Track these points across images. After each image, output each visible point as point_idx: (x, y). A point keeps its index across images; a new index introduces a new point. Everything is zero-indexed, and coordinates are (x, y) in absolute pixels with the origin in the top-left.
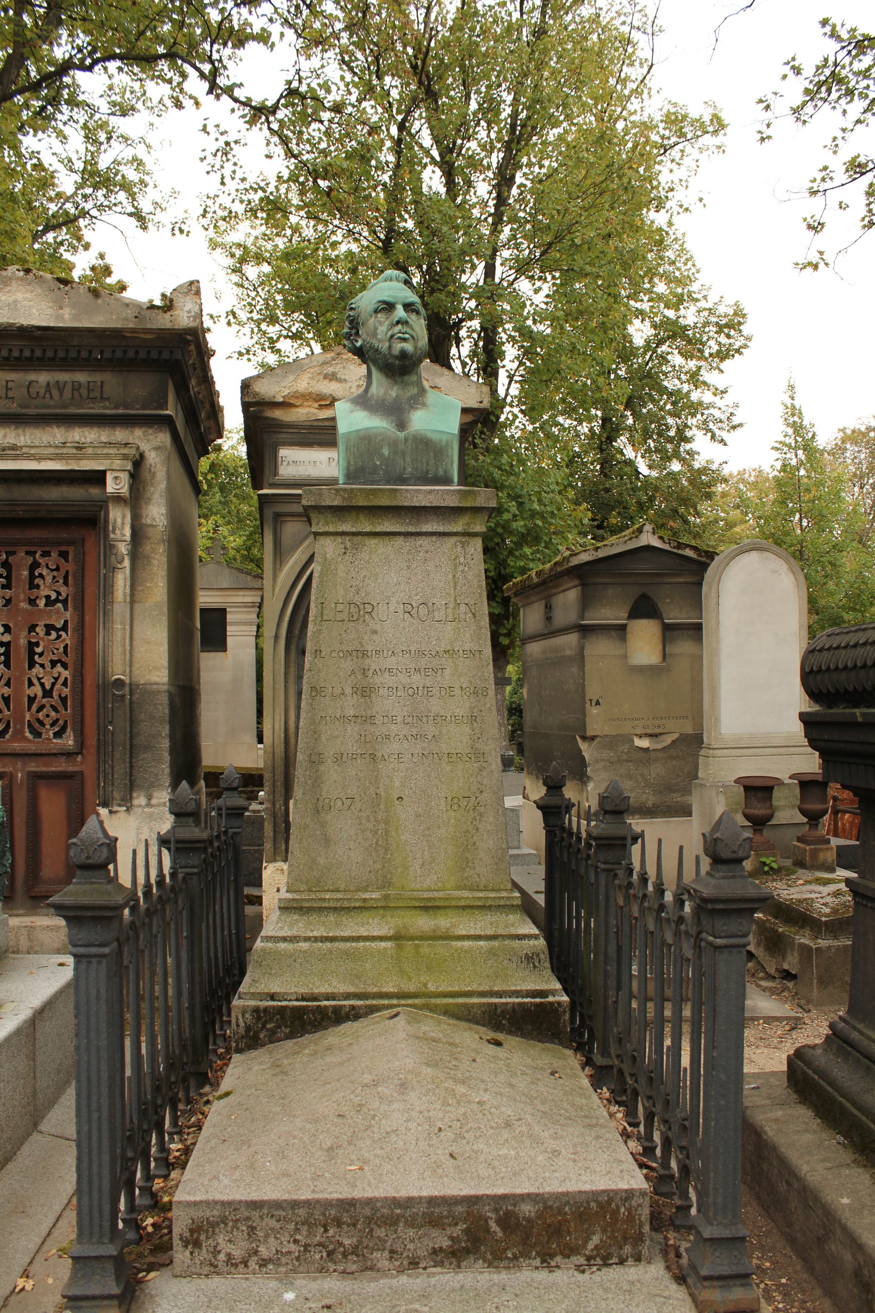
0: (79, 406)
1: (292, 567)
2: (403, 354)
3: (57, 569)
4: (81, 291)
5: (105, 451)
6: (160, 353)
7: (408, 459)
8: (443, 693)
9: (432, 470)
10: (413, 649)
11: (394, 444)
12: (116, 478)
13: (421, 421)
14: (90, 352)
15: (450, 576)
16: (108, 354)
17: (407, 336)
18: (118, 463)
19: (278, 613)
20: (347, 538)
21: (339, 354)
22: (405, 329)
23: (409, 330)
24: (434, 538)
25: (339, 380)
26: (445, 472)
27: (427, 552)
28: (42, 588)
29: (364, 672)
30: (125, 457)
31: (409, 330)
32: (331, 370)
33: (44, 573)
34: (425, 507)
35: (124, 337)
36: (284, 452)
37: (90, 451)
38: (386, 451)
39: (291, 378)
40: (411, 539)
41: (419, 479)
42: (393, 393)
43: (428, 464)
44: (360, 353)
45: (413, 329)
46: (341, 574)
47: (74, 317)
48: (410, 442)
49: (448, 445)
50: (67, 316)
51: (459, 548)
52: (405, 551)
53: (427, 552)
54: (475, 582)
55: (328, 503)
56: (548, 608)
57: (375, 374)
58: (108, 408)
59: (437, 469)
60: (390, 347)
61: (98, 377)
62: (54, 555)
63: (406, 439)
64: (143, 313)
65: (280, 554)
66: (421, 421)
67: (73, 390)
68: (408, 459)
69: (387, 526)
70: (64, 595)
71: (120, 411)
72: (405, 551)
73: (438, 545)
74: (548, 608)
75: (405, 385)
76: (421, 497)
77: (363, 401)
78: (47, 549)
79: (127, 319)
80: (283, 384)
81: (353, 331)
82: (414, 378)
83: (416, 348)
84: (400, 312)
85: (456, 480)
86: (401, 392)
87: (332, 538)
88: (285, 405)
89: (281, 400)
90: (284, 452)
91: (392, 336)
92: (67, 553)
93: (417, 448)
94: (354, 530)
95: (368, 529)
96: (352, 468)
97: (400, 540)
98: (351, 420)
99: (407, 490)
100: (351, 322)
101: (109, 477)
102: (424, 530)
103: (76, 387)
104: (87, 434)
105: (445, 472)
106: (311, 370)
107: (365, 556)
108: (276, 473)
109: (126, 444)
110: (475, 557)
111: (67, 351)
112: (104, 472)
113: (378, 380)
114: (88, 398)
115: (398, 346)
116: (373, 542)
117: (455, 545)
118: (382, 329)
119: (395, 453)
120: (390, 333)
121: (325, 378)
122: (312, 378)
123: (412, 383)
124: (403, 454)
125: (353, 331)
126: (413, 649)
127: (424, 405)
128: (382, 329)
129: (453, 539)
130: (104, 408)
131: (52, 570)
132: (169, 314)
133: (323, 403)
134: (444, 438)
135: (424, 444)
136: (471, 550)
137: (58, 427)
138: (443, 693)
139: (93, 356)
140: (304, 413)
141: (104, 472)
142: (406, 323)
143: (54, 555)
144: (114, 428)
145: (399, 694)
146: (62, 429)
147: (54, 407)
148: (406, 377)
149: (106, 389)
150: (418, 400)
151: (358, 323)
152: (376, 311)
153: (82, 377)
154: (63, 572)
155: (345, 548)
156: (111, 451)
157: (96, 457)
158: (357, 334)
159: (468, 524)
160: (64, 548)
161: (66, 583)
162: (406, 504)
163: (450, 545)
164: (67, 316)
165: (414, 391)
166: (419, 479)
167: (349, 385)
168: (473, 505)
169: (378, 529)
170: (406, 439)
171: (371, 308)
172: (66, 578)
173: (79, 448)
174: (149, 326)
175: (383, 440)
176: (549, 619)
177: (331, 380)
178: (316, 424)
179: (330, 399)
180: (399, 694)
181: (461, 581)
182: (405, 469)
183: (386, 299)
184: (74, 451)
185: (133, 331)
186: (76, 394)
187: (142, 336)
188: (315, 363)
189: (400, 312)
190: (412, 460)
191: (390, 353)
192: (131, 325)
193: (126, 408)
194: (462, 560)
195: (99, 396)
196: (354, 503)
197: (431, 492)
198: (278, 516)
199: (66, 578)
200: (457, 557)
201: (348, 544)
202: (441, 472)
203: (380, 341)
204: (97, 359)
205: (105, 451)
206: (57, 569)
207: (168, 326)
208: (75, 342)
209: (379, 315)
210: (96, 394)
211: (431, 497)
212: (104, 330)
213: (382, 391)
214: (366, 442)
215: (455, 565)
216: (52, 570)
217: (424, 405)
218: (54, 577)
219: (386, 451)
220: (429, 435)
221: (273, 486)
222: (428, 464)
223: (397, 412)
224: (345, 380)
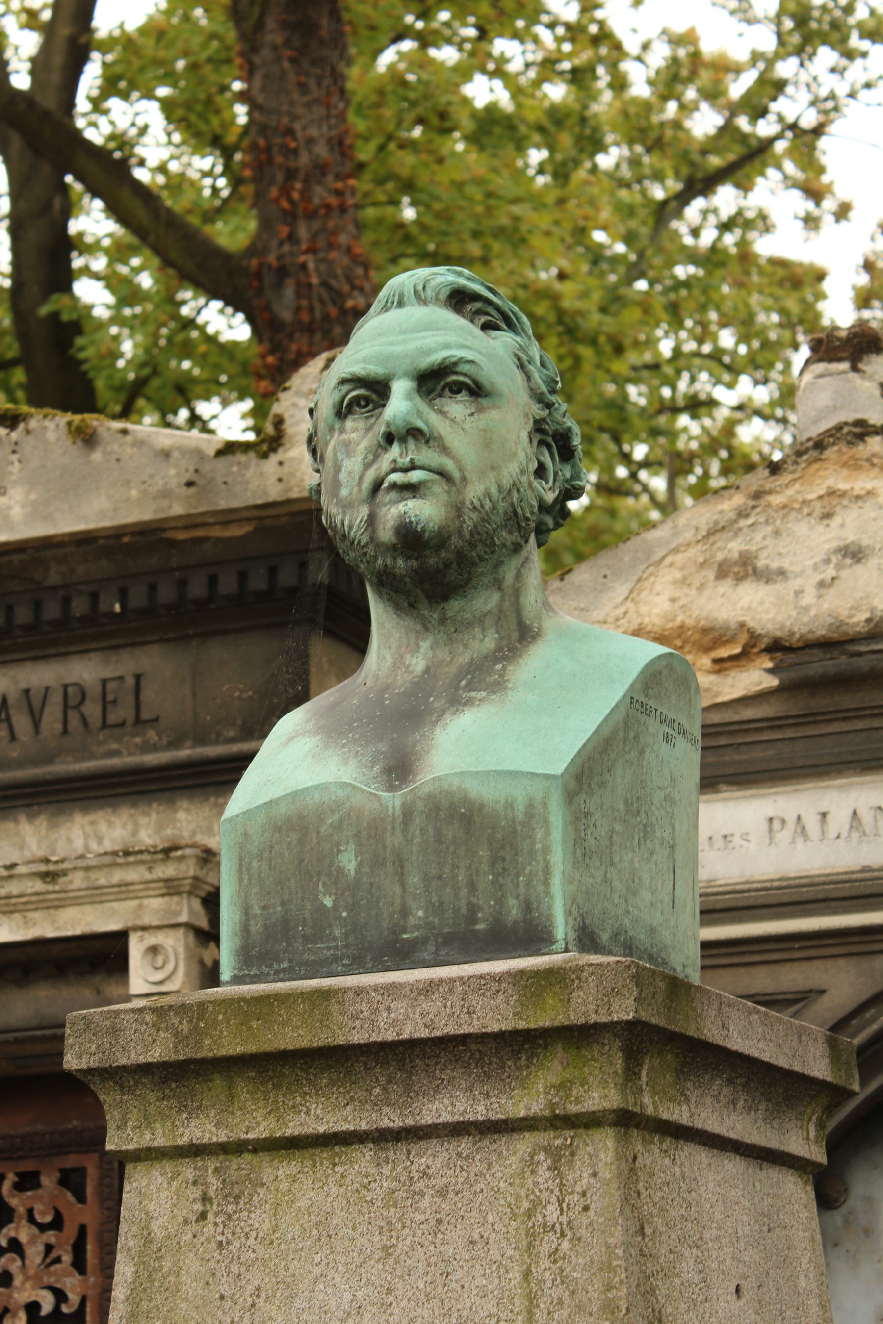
0: (85, 753)
3: (57, 1224)
4: (51, 436)
5: (118, 876)
6: (273, 571)
7: (414, 879)
9: (486, 904)
11: (371, 833)
12: (154, 950)
14: (94, 597)
15: (515, 1275)
16: (138, 598)
17: (415, 476)
18: (154, 907)
20: (211, 1164)
21: (758, 495)
24: (465, 1145)
25: (767, 576)
26: (527, 907)
27: (442, 1193)
28: (17, 1281)
30: (171, 888)
32: (734, 547)
33: (23, 1238)
34: (413, 1044)
35: (172, 543)
37: (77, 880)
38: (349, 861)
39: (621, 590)
40: (397, 1152)
41: (448, 940)
43: (472, 887)
45: (445, 449)
46: (190, 1286)
47: (36, 512)
48: (418, 821)
49: (534, 814)
50: (17, 512)
51: (543, 1174)
52: (377, 1193)
53: (442, 1193)
54: (595, 1294)
55: (136, 1056)
58: (155, 748)
59: (500, 901)
60: (372, 521)
61: (124, 665)
62: (48, 1181)
64: (206, 468)
67: (66, 707)
68: (414, 879)
69: (320, 1115)
70: (74, 1299)
71: (185, 753)
72: (377, 1193)
73: (477, 1166)
75: (453, 629)
76: (400, 1008)
78: (29, 1166)
79: (165, 494)
80: (598, 615)
82: (486, 601)
85: (561, 929)
86: (443, 654)
87: (169, 1166)
91: (377, 486)
92: (81, 1171)
93: (439, 838)
94: (222, 1136)
95: (261, 1132)
96: (256, 927)
97: (363, 1159)
99: (359, 991)
101: (136, 948)
102: (427, 1119)
103: (73, 698)
104: (103, 827)
105: (527, 907)
106: (679, 558)
107: (259, 1220)
109: (167, 851)
110: (597, 1202)
111: (38, 606)
112: (121, 937)
113: (382, 625)
114: (104, 725)
115: (396, 511)
116: (281, 1171)
117: (531, 1163)
119: (377, 863)
120: (371, 475)
121: (723, 571)
122: (684, 582)
123: (480, 621)
124: (400, 862)
129: (523, 1145)
130: (146, 748)
131: (43, 1228)
132: (274, 458)
133: (724, 652)
134: (520, 794)
136: (580, 1176)
137: (31, 817)
139: (103, 607)
141: (121, 937)
143: (48, 1181)
144: (171, 802)
146: (42, 822)
147: (20, 764)
148: (454, 605)
149: (147, 694)
153: (85, 670)
154: (70, 1231)
155: (205, 1199)
156: (133, 875)
157: (95, 895)
159: (563, 1086)
160: (72, 1161)
161: (79, 1265)
162: (357, 1038)
163: (514, 1162)
164: (17, 512)
166: (448, 940)
167: (794, 584)
168: (560, 1020)
169: (293, 1128)
170: (407, 813)
172: (79, 1249)
173: (49, 877)
174: (223, 504)
175: (338, 826)
177: (739, 579)
179: (743, 638)
181: (551, 1292)
182: (405, 912)
184: (39, 886)
185: (190, 522)
186: (73, 716)
187: (217, 532)
188: (688, 535)
189: (401, 403)
190: (426, 879)
192: (178, 510)
193: (201, 741)
194: (552, 1213)
195: (131, 719)
196: (208, 1049)
197: (429, 988)
199: (79, 1249)
200: (537, 1204)
201: (214, 1183)
202: (514, 911)
203: (347, 506)
204: (111, 614)
205: (118, 876)
206: (57, 1224)
207: (274, 493)
208: (54, 577)
209: (349, 424)
210: (123, 712)
211: (431, 1005)
212: (117, 534)
215: (531, 1235)
216: (43, 1228)
218: (49, 1248)
219: (349, 861)
220: (477, 790)
222: (472, 887)
224: (782, 573)
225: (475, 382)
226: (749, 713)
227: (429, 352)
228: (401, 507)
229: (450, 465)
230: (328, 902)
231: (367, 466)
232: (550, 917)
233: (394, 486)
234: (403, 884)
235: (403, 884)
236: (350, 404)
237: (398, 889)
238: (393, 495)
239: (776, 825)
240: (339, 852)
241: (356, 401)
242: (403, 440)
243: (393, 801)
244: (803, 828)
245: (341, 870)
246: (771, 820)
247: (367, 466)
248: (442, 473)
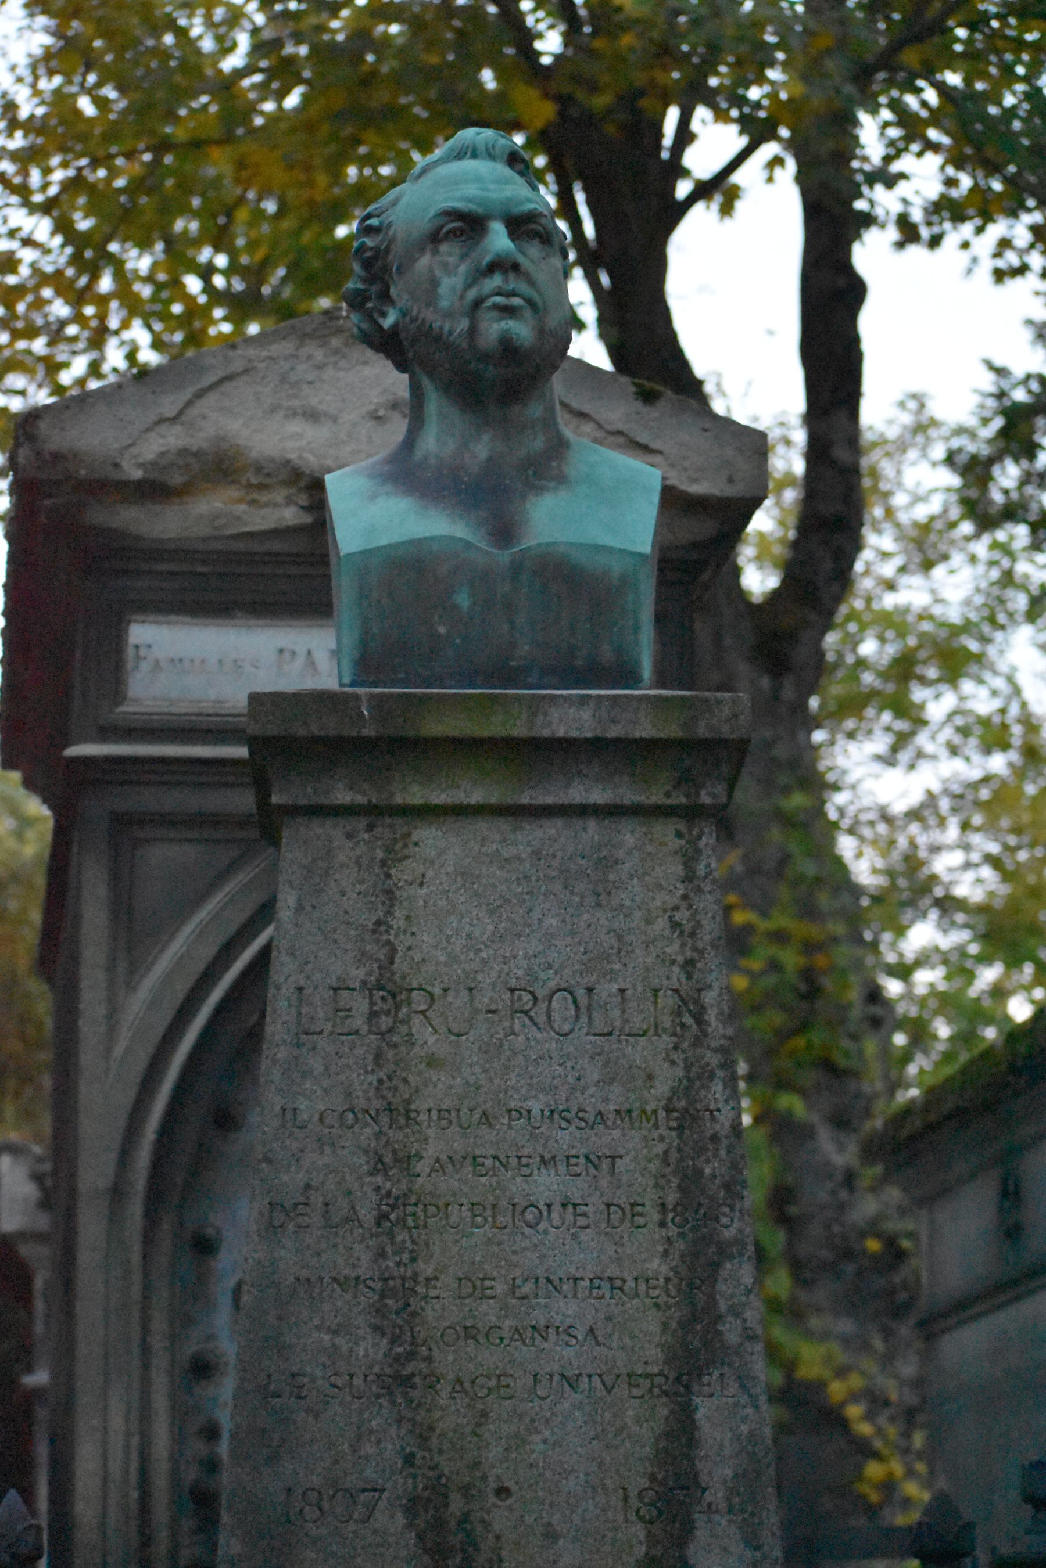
1: (168, 978)
2: (508, 348)
8: (615, 1218)
10: (536, 1107)
13: (552, 520)
17: (516, 301)
19: (122, 1122)
22: (513, 283)
23: (523, 287)
29: (405, 1161)
31: (523, 287)
36: (141, 633)
38: (463, 599)
42: (482, 449)
44: (391, 345)
45: (532, 283)
49: (626, 582)
56: (1011, 1194)
57: (434, 403)
60: (472, 332)
63: (516, 569)
65: (134, 935)
66: (552, 520)
74: (1011, 1194)
77: (404, 472)
81: (375, 289)
82: (535, 410)
83: (541, 332)
84: (499, 239)
85: (647, 671)
88: (153, 490)
89: (138, 474)
90: (141, 633)
91: (478, 303)
98: (368, 516)
99: (519, 698)
100: (367, 265)
108: (117, 691)
115: (493, 328)
118: (450, 285)
120: (472, 294)
125: (375, 289)
126: (536, 1107)
127: (561, 479)
128: (450, 285)
134: (617, 567)
135: (569, 581)
138: (615, 1218)
140: (213, 512)
142: (515, 267)
145: (501, 1220)
148: (516, 409)
150: (546, 467)
151: (386, 269)
152: (435, 238)
158: (385, 296)
165: (539, 443)
171: (424, 223)
176: (1012, 1232)
178: (241, 546)
180: (501, 1220)
183: (460, 205)
189: (499, 239)
191: (472, 346)
197: (584, 700)
198: (123, 823)
202: (607, 653)
209: (444, 248)
213: (451, 446)
214: (408, 569)
217: (561, 479)
221: (107, 733)
223: (491, 497)
225: (547, 233)
226: (277, 546)
227: (520, 203)
228: (503, 324)
229: (537, 299)
230: (442, 630)
231: (468, 286)
232: (638, 663)
233: (496, 307)
234: (512, 623)
235: (512, 623)
236: (448, 232)
237: (506, 627)
238: (495, 314)
239: (287, 655)
240: (454, 592)
241: (453, 232)
242: (505, 272)
243: (504, 557)
244: (313, 663)
245: (456, 607)
246: (281, 651)
247: (468, 286)
248: (529, 301)
